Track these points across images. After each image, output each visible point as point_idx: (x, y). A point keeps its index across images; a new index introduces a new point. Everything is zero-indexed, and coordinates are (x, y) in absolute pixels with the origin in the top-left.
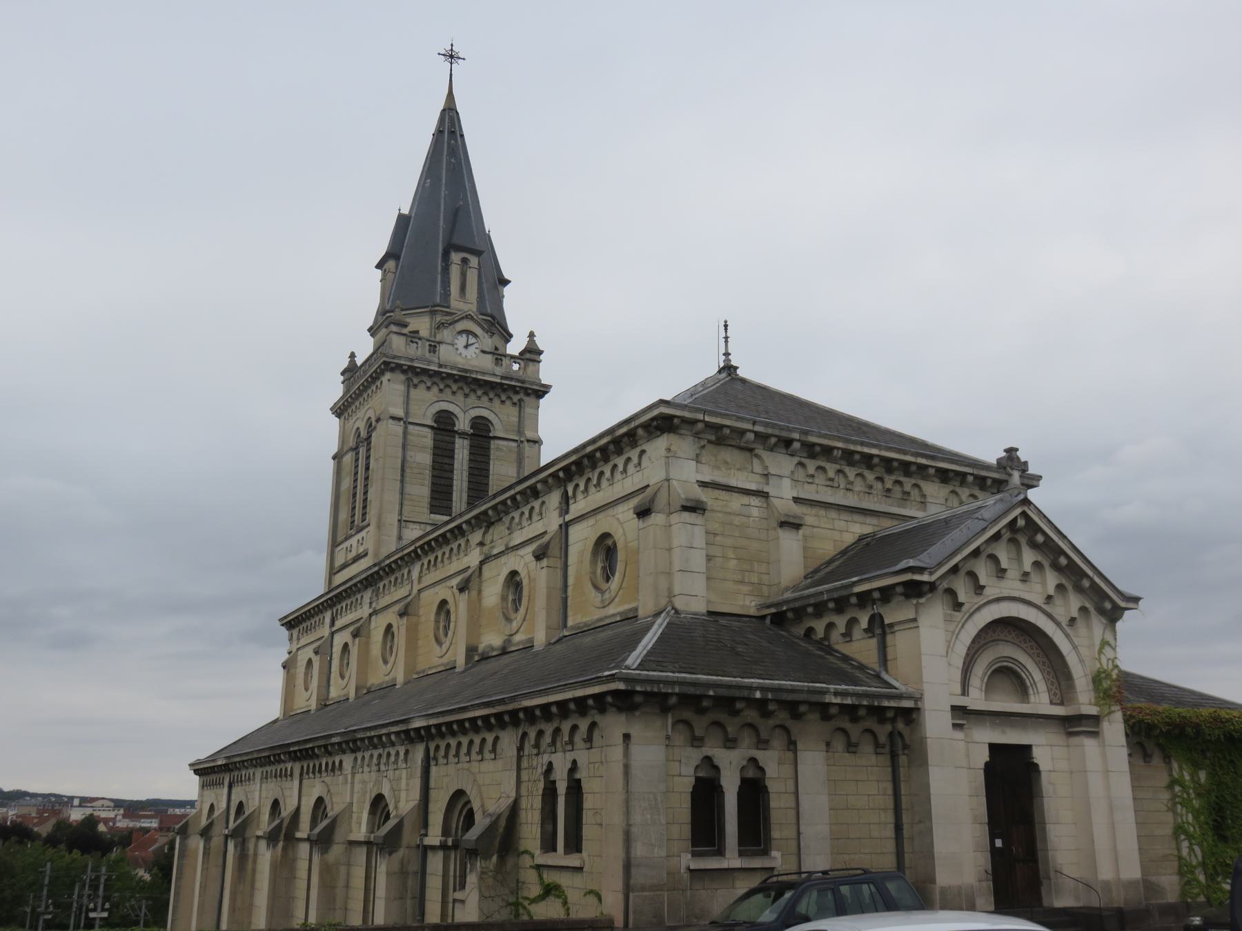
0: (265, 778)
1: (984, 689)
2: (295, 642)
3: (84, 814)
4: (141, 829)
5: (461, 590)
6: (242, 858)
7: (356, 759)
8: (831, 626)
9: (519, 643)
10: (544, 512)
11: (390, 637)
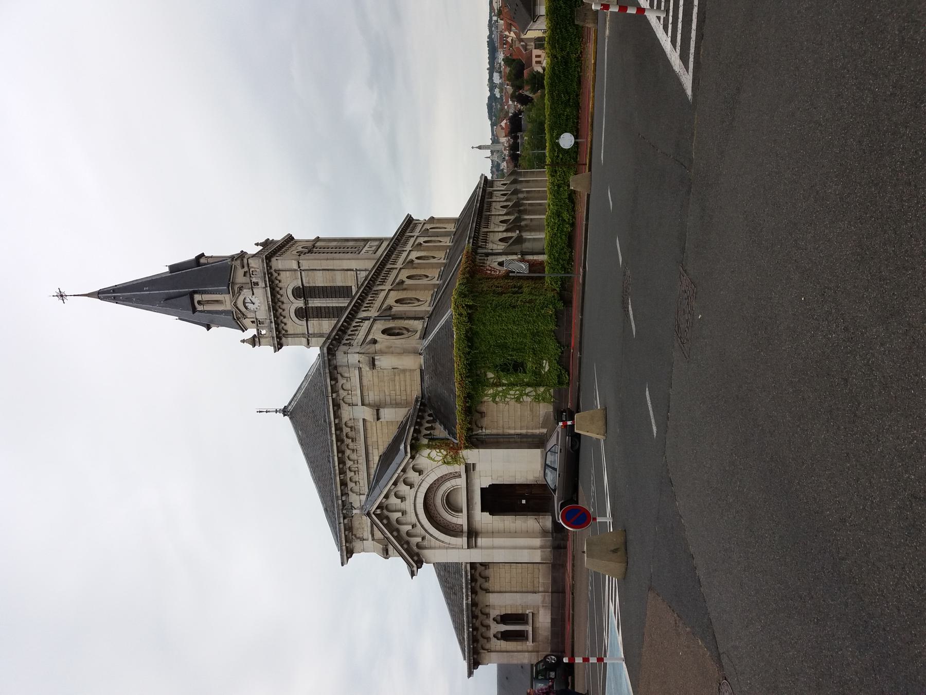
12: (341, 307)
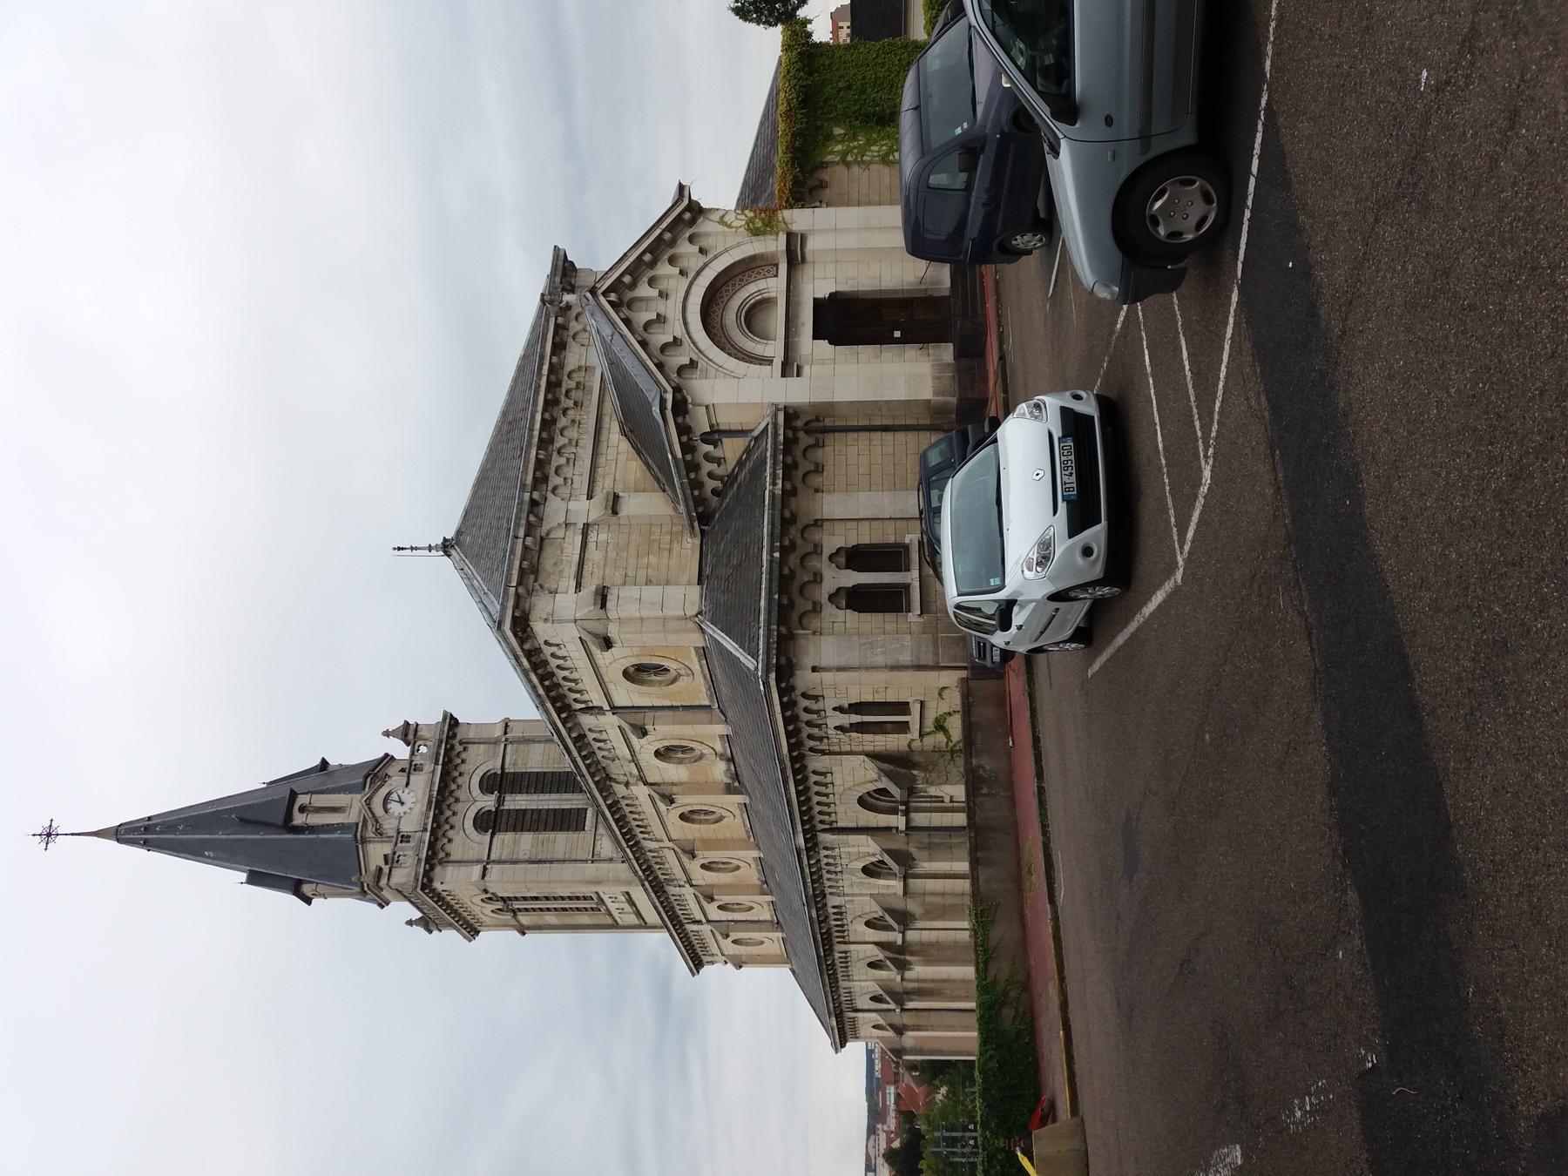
0: (848, 977)
1: (765, 341)
2: (716, 958)
3: (883, 1165)
4: (896, 1103)
5: (672, 801)
6: (921, 993)
7: (830, 894)
8: (711, 475)
9: (724, 748)
10: (599, 729)
11: (713, 865)
12: (563, 809)
